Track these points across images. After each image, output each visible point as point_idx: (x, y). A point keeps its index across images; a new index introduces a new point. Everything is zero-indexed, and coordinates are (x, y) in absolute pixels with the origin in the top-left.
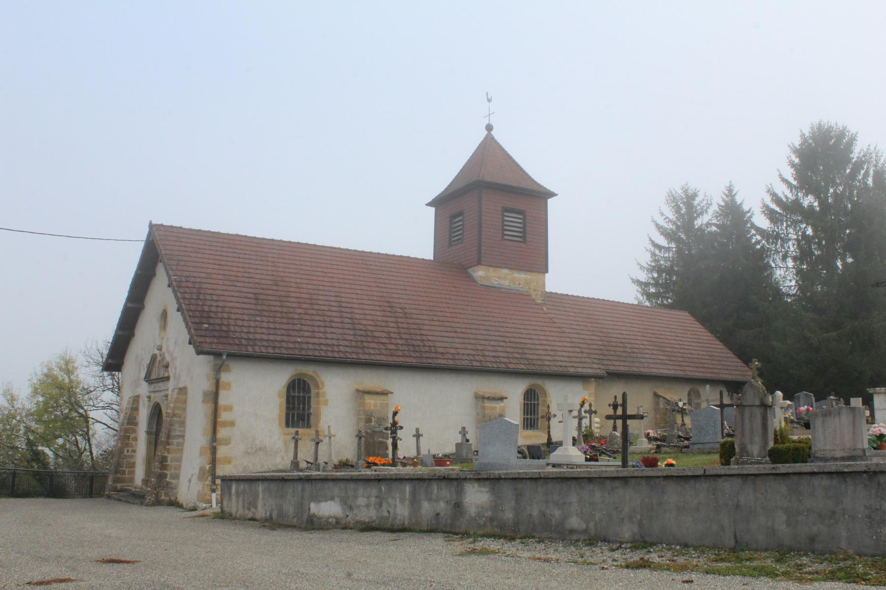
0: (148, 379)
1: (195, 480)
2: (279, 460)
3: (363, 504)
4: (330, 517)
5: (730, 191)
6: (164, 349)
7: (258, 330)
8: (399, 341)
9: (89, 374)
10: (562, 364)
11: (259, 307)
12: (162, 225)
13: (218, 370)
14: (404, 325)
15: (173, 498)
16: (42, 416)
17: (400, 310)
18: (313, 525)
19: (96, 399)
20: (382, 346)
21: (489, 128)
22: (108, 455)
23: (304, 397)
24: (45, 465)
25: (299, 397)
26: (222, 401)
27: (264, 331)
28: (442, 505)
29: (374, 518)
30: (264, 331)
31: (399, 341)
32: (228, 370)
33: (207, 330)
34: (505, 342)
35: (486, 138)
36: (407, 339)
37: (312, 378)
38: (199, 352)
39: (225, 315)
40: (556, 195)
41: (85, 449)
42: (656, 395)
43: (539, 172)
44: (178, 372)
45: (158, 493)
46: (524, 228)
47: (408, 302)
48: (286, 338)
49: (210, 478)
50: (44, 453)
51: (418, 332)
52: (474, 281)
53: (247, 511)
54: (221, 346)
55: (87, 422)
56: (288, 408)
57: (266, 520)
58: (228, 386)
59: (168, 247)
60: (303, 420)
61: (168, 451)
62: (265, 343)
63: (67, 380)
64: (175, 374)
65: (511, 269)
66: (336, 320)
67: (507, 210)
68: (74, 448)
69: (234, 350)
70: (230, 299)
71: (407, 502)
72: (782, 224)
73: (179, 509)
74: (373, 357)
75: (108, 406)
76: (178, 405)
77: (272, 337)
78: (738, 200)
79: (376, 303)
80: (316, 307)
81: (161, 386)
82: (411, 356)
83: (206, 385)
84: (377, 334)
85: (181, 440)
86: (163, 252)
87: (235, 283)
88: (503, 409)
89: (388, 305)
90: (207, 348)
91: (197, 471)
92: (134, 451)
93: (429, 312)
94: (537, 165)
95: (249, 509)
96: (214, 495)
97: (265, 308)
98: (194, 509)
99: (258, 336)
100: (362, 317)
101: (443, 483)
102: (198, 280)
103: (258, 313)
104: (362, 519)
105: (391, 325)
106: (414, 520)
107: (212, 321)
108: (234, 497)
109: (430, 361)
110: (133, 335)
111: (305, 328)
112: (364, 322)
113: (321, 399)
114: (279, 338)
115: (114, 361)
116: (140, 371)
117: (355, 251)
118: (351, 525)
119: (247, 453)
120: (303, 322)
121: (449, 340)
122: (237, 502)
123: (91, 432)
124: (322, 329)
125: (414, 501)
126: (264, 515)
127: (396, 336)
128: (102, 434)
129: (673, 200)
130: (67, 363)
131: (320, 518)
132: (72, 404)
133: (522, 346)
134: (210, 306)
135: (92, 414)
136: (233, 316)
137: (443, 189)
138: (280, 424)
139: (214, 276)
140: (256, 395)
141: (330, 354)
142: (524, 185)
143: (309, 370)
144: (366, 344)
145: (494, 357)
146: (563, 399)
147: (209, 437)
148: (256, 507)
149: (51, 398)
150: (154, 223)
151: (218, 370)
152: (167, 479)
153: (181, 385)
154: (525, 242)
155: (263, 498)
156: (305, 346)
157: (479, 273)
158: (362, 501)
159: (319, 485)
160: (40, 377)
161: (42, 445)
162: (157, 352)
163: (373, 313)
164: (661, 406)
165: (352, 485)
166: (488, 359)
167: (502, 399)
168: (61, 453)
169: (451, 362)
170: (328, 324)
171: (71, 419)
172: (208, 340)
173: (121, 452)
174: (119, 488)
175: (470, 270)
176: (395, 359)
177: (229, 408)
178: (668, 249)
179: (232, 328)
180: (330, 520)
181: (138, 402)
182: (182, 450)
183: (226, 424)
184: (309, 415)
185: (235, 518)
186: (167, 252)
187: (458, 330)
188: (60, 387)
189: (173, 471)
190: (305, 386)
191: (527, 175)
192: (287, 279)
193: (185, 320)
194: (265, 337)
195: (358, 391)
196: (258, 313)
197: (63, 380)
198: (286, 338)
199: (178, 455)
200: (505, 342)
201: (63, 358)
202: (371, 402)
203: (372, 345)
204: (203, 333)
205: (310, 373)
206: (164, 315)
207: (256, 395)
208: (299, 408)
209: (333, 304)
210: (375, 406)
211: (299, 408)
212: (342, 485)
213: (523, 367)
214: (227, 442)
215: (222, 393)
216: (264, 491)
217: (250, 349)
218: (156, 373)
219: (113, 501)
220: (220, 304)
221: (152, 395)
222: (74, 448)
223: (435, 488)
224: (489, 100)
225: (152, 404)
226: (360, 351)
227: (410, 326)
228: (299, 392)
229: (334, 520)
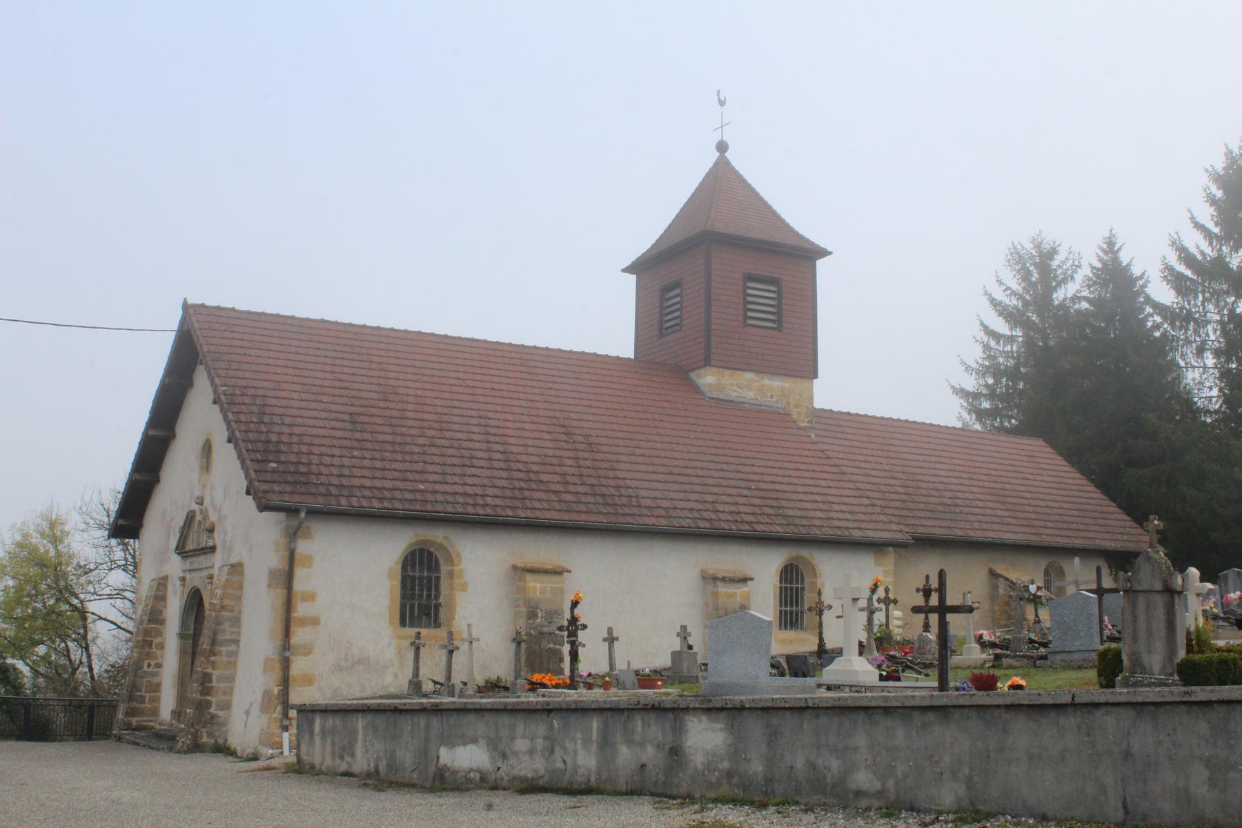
0: (181, 550)
1: (255, 710)
2: (389, 679)
3: (524, 749)
4: (471, 770)
5: (1110, 243)
6: (207, 502)
7: (356, 472)
8: (581, 489)
9: (87, 543)
10: (841, 524)
11: (358, 435)
12: (203, 306)
13: (293, 535)
14: (588, 463)
15: (221, 741)
16: (13, 609)
17: (581, 439)
18: (444, 782)
19: (99, 582)
20: (553, 497)
21: (722, 147)
22: (117, 671)
23: (429, 579)
24: (17, 688)
25: (421, 578)
26: (299, 586)
27: (366, 473)
28: (650, 750)
29: (542, 772)
30: (366, 473)
31: (581, 489)
32: (308, 536)
33: (274, 471)
35: (717, 164)
37: (441, 547)
38: (263, 508)
39: (304, 449)
40: (830, 253)
41: (81, 663)
42: (993, 574)
43: (802, 215)
44: (228, 538)
45: (197, 733)
46: (779, 306)
48: (400, 485)
49: (279, 708)
50: (15, 669)
51: (611, 474)
52: (696, 389)
53: (338, 761)
54: (298, 498)
55: (85, 619)
56: (403, 596)
57: (369, 775)
58: (308, 561)
59: (212, 341)
60: (428, 615)
61: (213, 664)
62: (367, 493)
63: (52, 553)
64: (224, 542)
65: (757, 372)
66: (480, 454)
67: (750, 278)
68: (63, 661)
69: (319, 503)
70: (312, 422)
71: (594, 747)
72: (1196, 297)
73: (231, 758)
74: (539, 514)
75: (118, 594)
76: (230, 591)
77: (378, 483)
78: (1124, 258)
80: (449, 434)
81: (202, 561)
83: (273, 559)
84: (545, 477)
85: (233, 648)
86: (205, 348)
87: (320, 397)
88: (747, 596)
89: (563, 430)
90: (275, 500)
91: (258, 696)
92: (159, 666)
94: (797, 199)
95: (342, 758)
96: (286, 735)
97: (367, 436)
98: (255, 758)
99: (356, 482)
100: (521, 449)
101: (653, 716)
102: (260, 392)
103: (356, 444)
104: (522, 774)
105: (568, 462)
106: (604, 776)
107: (282, 457)
108: (318, 740)
109: (630, 520)
110: (157, 480)
111: (430, 468)
112: (524, 458)
113: (456, 581)
114: (389, 484)
115: (129, 519)
116: (169, 535)
117: (510, 345)
118: (505, 783)
119: (338, 668)
120: (428, 459)
122: (324, 746)
123: (90, 636)
124: (459, 471)
125: (606, 744)
126: (365, 768)
127: (575, 480)
128: (108, 640)
129: (1018, 260)
130: (53, 524)
131: (455, 772)
132: (60, 592)
134: (280, 434)
135: (92, 607)
136: (316, 450)
138: (391, 622)
139: (285, 386)
140: (353, 574)
141: (470, 510)
143: (437, 535)
144: (527, 493)
146: (842, 580)
147: (278, 643)
148: (353, 755)
149: (27, 582)
150: (190, 302)
151: (293, 535)
152: (212, 710)
153: (234, 560)
154: (779, 329)
155: (365, 741)
156: (430, 497)
157: (708, 379)
158: (521, 745)
159: (453, 719)
160: (10, 547)
161: (13, 656)
162: (195, 507)
163: (538, 443)
164: (1001, 591)
165: (506, 720)
167: (745, 580)
168: (42, 669)
169: (664, 522)
170: (467, 462)
171: (60, 614)
172: (277, 488)
173: (138, 666)
174: (134, 723)
175: (693, 375)
177: (310, 597)
178: (1011, 339)
179: (314, 469)
180: (472, 775)
181: (165, 586)
182: (235, 663)
183: (304, 622)
184: (437, 607)
185: (320, 773)
186: (212, 348)
188: (42, 564)
189: (221, 697)
190: (430, 561)
191: (783, 221)
192: (401, 391)
193: (240, 456)
194: (367, 483)
195: (515, 568)
196: (356, 444)
197: (47, 552)
198: (400, 485)
199: (228, 672)
201: (45, 517)
202: (536, 585)
203: (537, 495)
204: (269, 477)
205: (439, 541)
206: (207, 448)
207: (353, 574)
208: (421, 595)
209: (475, 429)
210: (542, 592)
211: (421, 596)
212: (489, 718)
213: (779, 528)
214: (307, 650)
215: (299, 572)
216: (365, 728)
217: (343, 501)
218: (194, 540)
219: (124, 745)
220: (296, 430)
221: (188, 576)
222: (63, 661)
223: (638, 723)
224: (722, 103)
225: (187, 590)
226: (519, 504)
227: (598, 464)
228: (421, 570)
229: (478, 776)
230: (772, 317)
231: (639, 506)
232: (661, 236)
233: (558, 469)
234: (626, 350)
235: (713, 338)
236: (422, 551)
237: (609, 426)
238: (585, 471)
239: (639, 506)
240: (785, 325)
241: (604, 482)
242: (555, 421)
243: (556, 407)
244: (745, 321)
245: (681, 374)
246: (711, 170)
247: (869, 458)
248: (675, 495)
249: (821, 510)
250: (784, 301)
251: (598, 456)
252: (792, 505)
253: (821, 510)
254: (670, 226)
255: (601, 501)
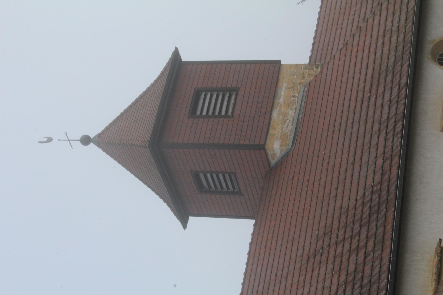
8: (363, 236)
14: (341, 233)
17: (320, 243)
20: (370, 257)
21: (86, 140)
31: (363, 236)
34: (370, 98)
35: (99, 145)
36: (361, 226)
40: (176, 49)
43: (144, 73)
46: (218, 90)
47: (309, 234)
51: (351, 212)
65: (272, 107)
67: (193, 112)
74: (385, 268)
79: (309, 275)
82: (386, 215)
84: (352, 267)
89: (311, 260)
93: (325, 204)
94: (134, 77)
105: (339, 250)
121: (364, 169)
127: (355, 242)
133: (376, 74)
137: (165, 205)
142: (160, 90)
144: (366, 281)
145: (390, 107)
154: (237, 90)
157: (276, 147)
163: (321, 279)
166: (393, 112)
169: (396, 160)
176: (388, 235)
187: (351, 161)
191: (149, 89)
200: (370, 98)
203: (367, 271)
213: (405, 67)
224: (50, 140)
227: (342, 224)
230: (227, 96)
231: (381, 183)
232: (157, 194)
233: (345, 257)
234: (248, 225)
235: (242, 142)
236: (439, 60)
237: (311, 221)
238: (348, 234)
239: (381, 183)
240: (234, 85)
241: (358, 217)
242: (304, 267)
243: (292, 268)
244: (229, 117)
245: (272, 172)
246: (104, 150)
247: (350, 21)
248: (373, 156)
249: (391, 37)
250: (214, 86)
251: (335, 226)
252: (385, 61)
253: (391, 37)
254: (149, 186)
255: (375, 216)
